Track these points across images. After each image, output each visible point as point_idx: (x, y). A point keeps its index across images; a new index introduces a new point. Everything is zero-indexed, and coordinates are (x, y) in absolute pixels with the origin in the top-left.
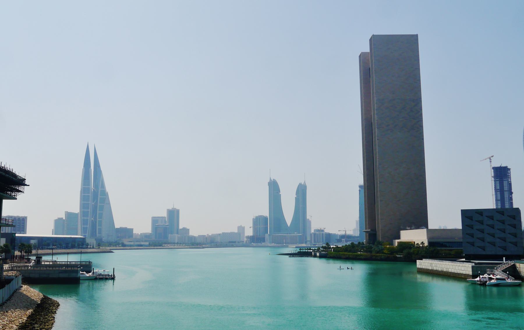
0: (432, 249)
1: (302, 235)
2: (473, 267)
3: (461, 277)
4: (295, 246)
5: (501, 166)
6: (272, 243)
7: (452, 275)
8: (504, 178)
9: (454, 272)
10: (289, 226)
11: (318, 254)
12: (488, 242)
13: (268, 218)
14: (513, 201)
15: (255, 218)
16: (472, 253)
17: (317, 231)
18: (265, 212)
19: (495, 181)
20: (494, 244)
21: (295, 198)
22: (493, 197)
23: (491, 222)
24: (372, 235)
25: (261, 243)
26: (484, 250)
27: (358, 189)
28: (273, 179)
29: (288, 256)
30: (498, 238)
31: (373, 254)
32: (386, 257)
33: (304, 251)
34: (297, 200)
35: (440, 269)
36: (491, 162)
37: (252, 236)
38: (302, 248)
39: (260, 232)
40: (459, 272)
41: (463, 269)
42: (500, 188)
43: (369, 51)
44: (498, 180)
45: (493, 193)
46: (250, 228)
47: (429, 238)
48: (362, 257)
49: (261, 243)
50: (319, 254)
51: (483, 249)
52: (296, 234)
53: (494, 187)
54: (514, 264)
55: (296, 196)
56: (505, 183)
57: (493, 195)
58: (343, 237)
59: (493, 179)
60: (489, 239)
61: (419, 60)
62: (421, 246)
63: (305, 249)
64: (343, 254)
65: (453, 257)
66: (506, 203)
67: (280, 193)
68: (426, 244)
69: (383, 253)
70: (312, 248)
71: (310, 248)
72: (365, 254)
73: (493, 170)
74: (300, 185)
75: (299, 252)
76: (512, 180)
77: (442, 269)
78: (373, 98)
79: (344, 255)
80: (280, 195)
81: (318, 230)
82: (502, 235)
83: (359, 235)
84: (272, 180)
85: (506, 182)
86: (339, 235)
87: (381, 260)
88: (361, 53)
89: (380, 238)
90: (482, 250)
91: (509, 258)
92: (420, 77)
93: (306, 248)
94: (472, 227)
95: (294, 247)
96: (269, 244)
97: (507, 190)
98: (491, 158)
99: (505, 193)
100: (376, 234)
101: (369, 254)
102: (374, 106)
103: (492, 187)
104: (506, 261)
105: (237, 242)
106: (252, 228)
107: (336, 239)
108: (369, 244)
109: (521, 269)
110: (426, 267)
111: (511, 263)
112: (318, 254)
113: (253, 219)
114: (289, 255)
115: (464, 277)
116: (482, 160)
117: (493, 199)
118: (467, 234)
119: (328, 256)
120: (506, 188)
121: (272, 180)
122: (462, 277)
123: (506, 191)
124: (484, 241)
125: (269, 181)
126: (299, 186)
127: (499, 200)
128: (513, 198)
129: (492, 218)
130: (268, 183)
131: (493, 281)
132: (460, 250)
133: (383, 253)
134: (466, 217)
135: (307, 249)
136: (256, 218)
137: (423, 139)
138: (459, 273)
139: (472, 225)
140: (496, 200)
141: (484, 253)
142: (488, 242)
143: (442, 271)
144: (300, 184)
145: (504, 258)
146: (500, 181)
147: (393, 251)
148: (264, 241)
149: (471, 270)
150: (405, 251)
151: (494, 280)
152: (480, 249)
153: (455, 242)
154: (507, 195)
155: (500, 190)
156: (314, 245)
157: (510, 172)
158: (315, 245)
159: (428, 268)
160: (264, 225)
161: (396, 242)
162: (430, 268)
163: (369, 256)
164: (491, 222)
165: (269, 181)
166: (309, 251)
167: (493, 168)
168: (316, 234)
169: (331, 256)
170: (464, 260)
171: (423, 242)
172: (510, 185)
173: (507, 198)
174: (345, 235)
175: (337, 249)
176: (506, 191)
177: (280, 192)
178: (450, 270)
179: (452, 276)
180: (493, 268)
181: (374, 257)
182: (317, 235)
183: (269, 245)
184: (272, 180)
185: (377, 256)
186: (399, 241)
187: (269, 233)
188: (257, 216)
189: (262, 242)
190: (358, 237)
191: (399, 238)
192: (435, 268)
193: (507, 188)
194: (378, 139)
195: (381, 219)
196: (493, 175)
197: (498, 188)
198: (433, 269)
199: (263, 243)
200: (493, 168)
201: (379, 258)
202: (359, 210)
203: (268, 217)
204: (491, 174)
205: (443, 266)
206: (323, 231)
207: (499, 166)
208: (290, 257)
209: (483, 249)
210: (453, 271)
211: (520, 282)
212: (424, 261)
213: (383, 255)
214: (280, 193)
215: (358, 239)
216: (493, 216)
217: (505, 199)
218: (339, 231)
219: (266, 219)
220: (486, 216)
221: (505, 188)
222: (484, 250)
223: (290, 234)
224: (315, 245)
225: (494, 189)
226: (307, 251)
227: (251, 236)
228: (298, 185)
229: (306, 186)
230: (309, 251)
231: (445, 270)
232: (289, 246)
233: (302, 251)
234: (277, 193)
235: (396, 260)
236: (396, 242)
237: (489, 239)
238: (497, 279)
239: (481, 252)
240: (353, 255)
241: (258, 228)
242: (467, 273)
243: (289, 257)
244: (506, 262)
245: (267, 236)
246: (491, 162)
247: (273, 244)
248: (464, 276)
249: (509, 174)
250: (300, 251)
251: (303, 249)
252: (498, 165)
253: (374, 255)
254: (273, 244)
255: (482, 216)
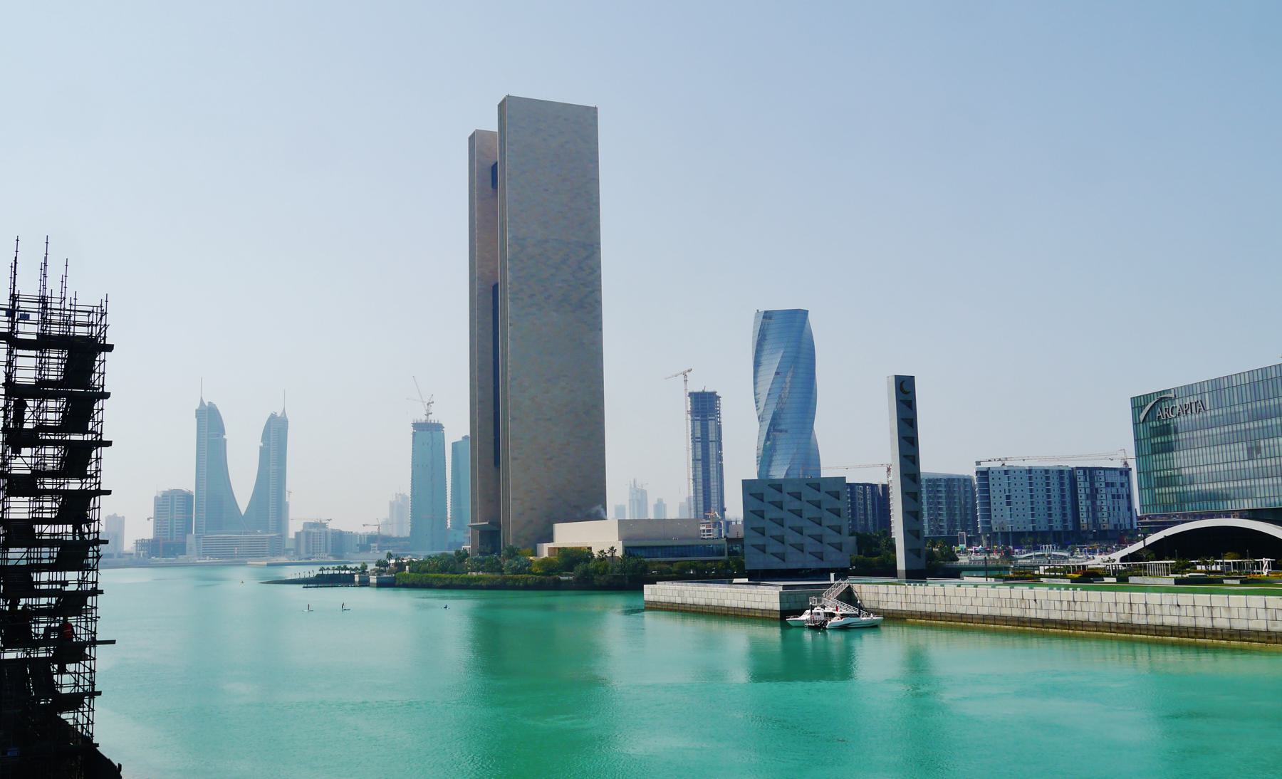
0: (633, 561)
1: (279, 536)
2: (781, 594)
3: (753, 615)
4: (266, 563)
5: (703, 391)
6: (204, 556)
7: (733, 613)
8: (710, 416)
9: (736, 606)
10: (243, 513)
11: (373, 580)
12: (791, 545)
13: (193, 496)
14: (724, 462)
15: (160, 496)
16: (761, 567)
17: (311, 527)
18: (188, 483)
19: (693, 421)
20: (801, 548)
21: (261, 447)
22: (688, 454)
23: (796, 505)
24: (490, 536)
25: (177, 557)
26: (784, 560)
27: (411, 430)
28: (210, 403)
29: (302, 586)
30: (809, 536)
31: (508, 574)
32: (537, 581)
33: (331, 572)
34: (264, 452)
35: (702, 602)
36: (686, 381)
37: (152, 541)
38: (326, 567)
39: (172, 531)
40: (748, 605)
41: (758, 598)
42: (702, 435)
43: (497, 130)
44: (698, 420)
45: (688, 445)
46: (148, 519)
47: (623, 538)
48: (484, 583)
49: (177, 557)
50: (377, 578)
51: (782, 557)
52: (260, 533)
53: (690, 433)
54: (849, 586)
55: (262, 444)
56: (711, 425)
57: (688, 449)
58: (372, 538)
59: (689, 417)
60: (792, 538)
61: (598, 162)
62: (609, 555)
63: (334, 569)
64: (437, 577)
65: (723, 575)
66: (711, 465)
67: (225, 437)
68: (619, 553)
69: (530, 572)
70: (349, 566)
71: (345, 567)
72: (489, 575)
73: (689, 399)
74: (273, 417)
75: (318, 576)
76: (722, 420)
77: (708, 602)
78: (503, 231)
79: (440, 579)
80: (225, 440)
81: (315, 525)
82: (817, 530)
83: (411, 533)
84: (207, 404)
85: (713, 422)
86: (360, 536)
87: (527, 587)
88: (474, 130)
89: (509, 538)
90: (780, 561)
91: (842, 573)
92: (598, 198)
93: (336, 567)
94: (761, 515)
95: (264, 565)
96: (197, 558)
97: (714, 439)
98: (687, 374)
99: (710, 446)
100: (499, 532)
101: (497, 575)
102: (504, 250)
103: (687, 433)
104: (836, 580)
105: (116, 555)
106: (152, 520)
107: (358, 545)
108: (481, 553)
109: (863, 594)
110: (667, 600)
111: (844, 584)
112: (373, 580)
113: (156, 499)
114: (305, 584)
115: (761, 615)
116: (670, 378)
117: (688, 456)
118: (752, 528)
119: (397, 583)
120: (712, 436)
121: (207, 404)
122: (757, 615)
123: (712, 441)
124: (821, 542)
125: (197, 406)
126: (269, 419)
127: (699, 460)
128: (723, 455)
129: (798, 496)
130: (197, 410)
131: (835, 620)
132: (688, 563)
133: (530, 572)
134: (751, 494)
135: (339, 569)
136: (163, 496)
137: (601, 329)
138: (750, 607)
139: (763, 511)
140: (693, 460)
141: (783, 566)
142: (791, 545)
143: (684, 604)
144: (273, 417)
145: (832, 575)
146: (701, 420)
147: (549, 567)
148: (184, 553)
149: (777, 599)
150: (580, 568)
151: (838, 617)
152: (776, 560)
153: (673, 546)
154: (714, 449)
155: (702, 439)
156: (306, 559)
157: (719, 404)
158: (309, 559)
159: (673, 600)
160: (183, 514)
161: (545, 550)
162: (679, 600)
163: (499, 580)
164: (796, 505)
165: (199, 405)
166: (343, 572)
167: (691, 394)
168: (310, 533)
169: (407, 582)
170: (746, 580)
171: (612, 548)
172: (719, 429)
173: (714, 456)
174: (376, 536)
175: (416, 567)
176: (712, 441)
177: (223, 432)
178: (727, 603)
179: (745, 616)
180: (819, 595)
181: (510, 583)
182: (313, 536)
183: (198, 561)
184: (205, 406)
185: (517, 580)
186: (551, 545)
187: (195, 533)
188: (167, 490)
189: (177, 554)
190: (405, 539)
191: (550, 538)
192: (690, 601)
193: (714, 435)
194: (510, 325)
195: (513, 499)
196: (689, 409)
197: (699, 435)
198: (684, 602)
199: (181, 557)
200: (691, 394)
201: (521, 584)
202: (412, 480)
203: (194, 494)
204: (687, 407)
205: (711, 595)
206: (324, 525)
207: (701, 390)
208: (307, 587)
209: (782, 557)
210: (734, 604)
211: (878, 620)
212: (660, 586)
213: (530, 576)
214: (225, 437)
215: (407, 542)
216: (800, 493)
217: (711, 457)
218: (364, 525)
219: (187, 497)
220: (788, 493)
221: (710, 435)
222: (784, 560)
223: (245, 533)
224: (309, 559)
225: (690, 437)
226: (337, 572)
227: (149, 540)
228: (267, 419)
229: (287, 421)
230: (343, 572)
231: (714, 603)
232: (248, 563)
233: (325, 572)
234: (218, 435)
235: (558, 586)
236: (545, 550)
237: (792, 538)
238: (843, 616)
239: (776, 564)
240: (462, 578)
241: (167, 520)
242: (769, 606)
243: (304, 587)
244: (836, 582)
245: (191, 539)
246: (686, 381)
247: (208, 560)
248: (762, 613)
249: (717, 407)
250: (321, 573)
251: (328, 569)
252: (698, 389)
253: (512, 579)
254: (208, 558)
255: (781, 492)
